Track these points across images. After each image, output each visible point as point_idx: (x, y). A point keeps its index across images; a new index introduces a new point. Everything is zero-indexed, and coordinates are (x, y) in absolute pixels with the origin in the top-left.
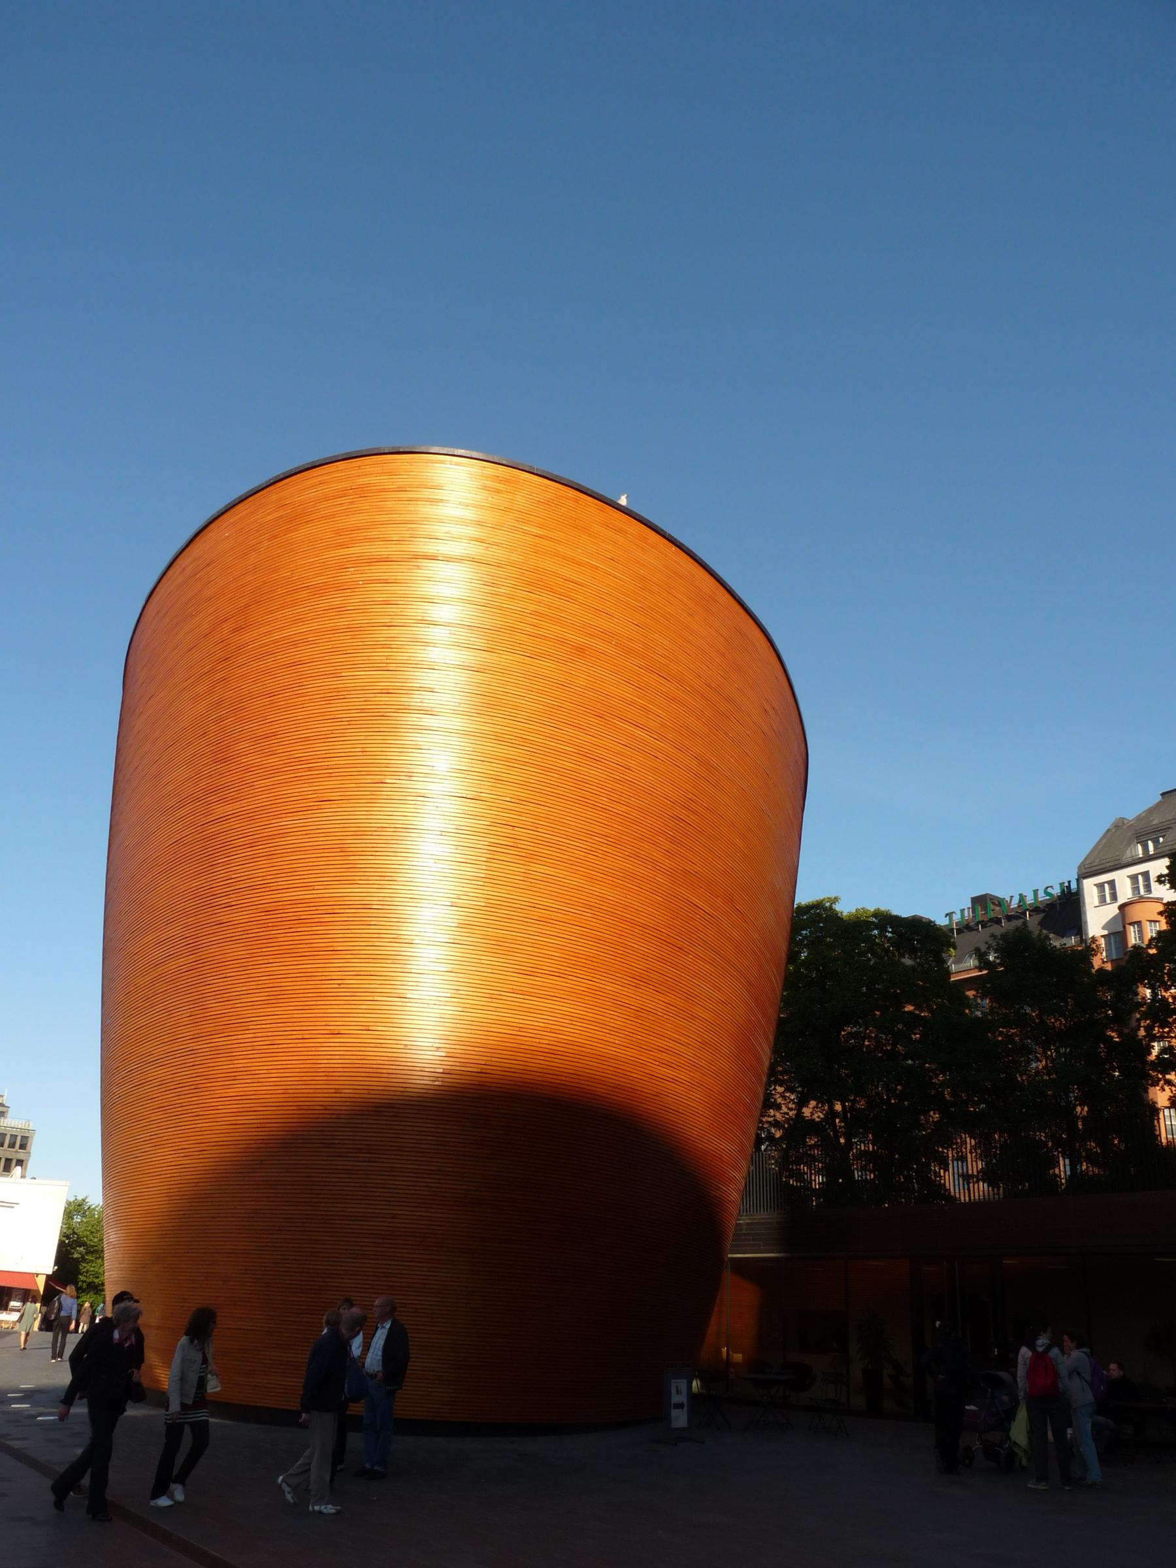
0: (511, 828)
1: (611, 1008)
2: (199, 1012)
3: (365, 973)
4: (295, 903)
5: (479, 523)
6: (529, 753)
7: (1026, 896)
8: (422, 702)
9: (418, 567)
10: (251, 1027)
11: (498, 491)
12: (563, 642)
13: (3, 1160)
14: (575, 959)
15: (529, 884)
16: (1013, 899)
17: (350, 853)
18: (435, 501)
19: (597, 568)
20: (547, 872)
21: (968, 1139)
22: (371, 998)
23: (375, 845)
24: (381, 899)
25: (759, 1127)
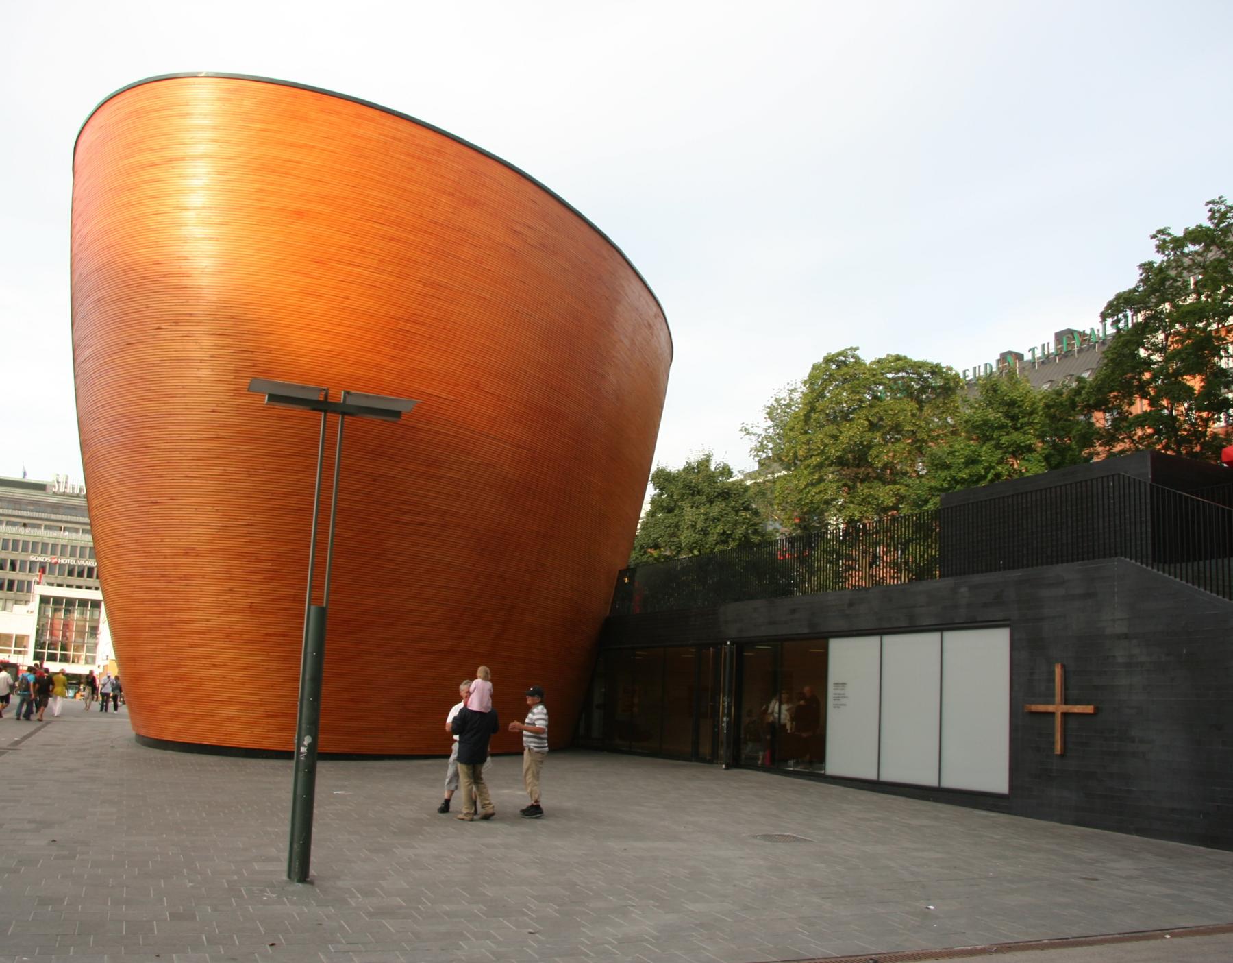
5: (215, 128)
7: (1084, 331)
8: (180, 268)
9: (173, 168)
11: (229, 100)
13: (2, 540)
16: (1050, 345)
18: (183, 116)
19: (313, 147)
25: (968, 388)
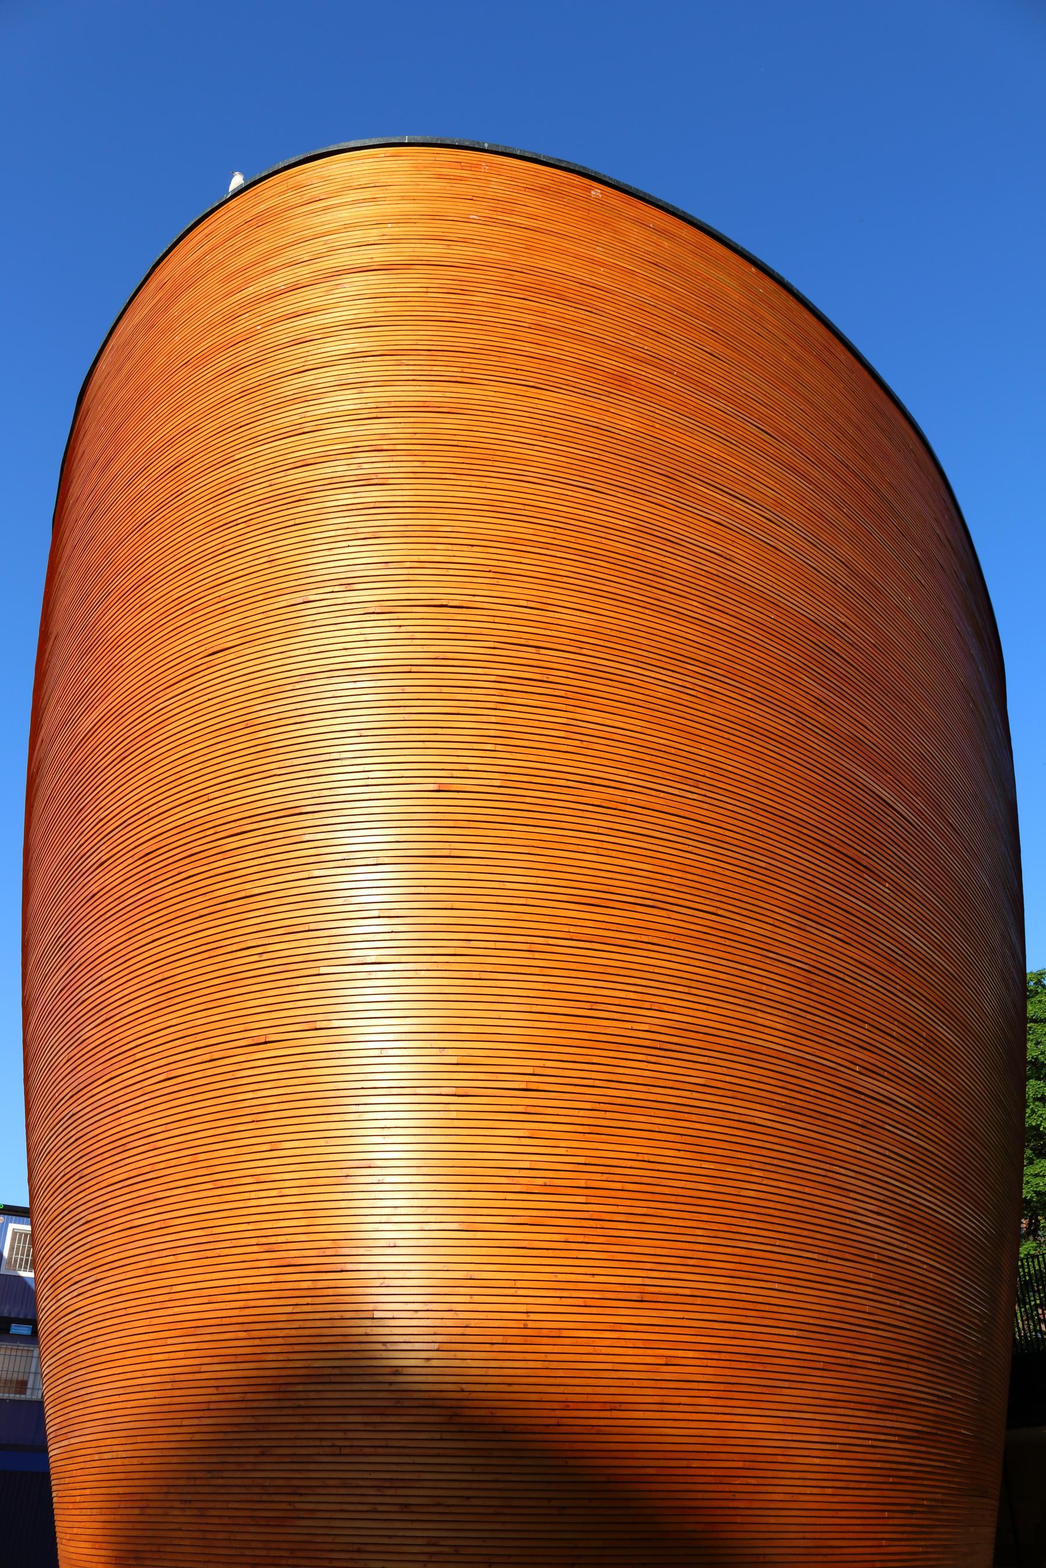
0: (534, 650)
1: (760, 965)
2: (76, 1051)
3: (301, 928)
4: (182, 829)
6: (552, 529)
10: (138, 1056)
12: (590, 367)
14: (679, 874)
15: (578, 743)
17: (261, 727)
20: (608, 722)
21: (1042, 1225)
22: (315, 971)
23: (298, 706)
24: (315, 794)
